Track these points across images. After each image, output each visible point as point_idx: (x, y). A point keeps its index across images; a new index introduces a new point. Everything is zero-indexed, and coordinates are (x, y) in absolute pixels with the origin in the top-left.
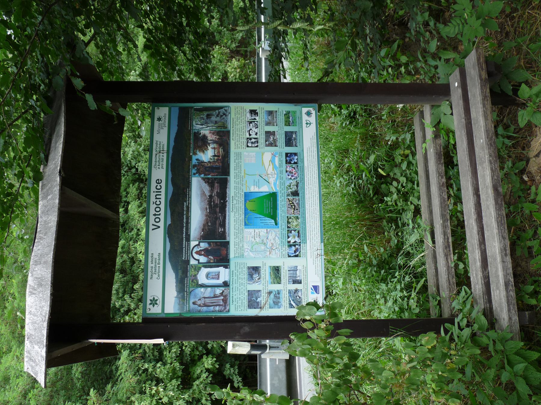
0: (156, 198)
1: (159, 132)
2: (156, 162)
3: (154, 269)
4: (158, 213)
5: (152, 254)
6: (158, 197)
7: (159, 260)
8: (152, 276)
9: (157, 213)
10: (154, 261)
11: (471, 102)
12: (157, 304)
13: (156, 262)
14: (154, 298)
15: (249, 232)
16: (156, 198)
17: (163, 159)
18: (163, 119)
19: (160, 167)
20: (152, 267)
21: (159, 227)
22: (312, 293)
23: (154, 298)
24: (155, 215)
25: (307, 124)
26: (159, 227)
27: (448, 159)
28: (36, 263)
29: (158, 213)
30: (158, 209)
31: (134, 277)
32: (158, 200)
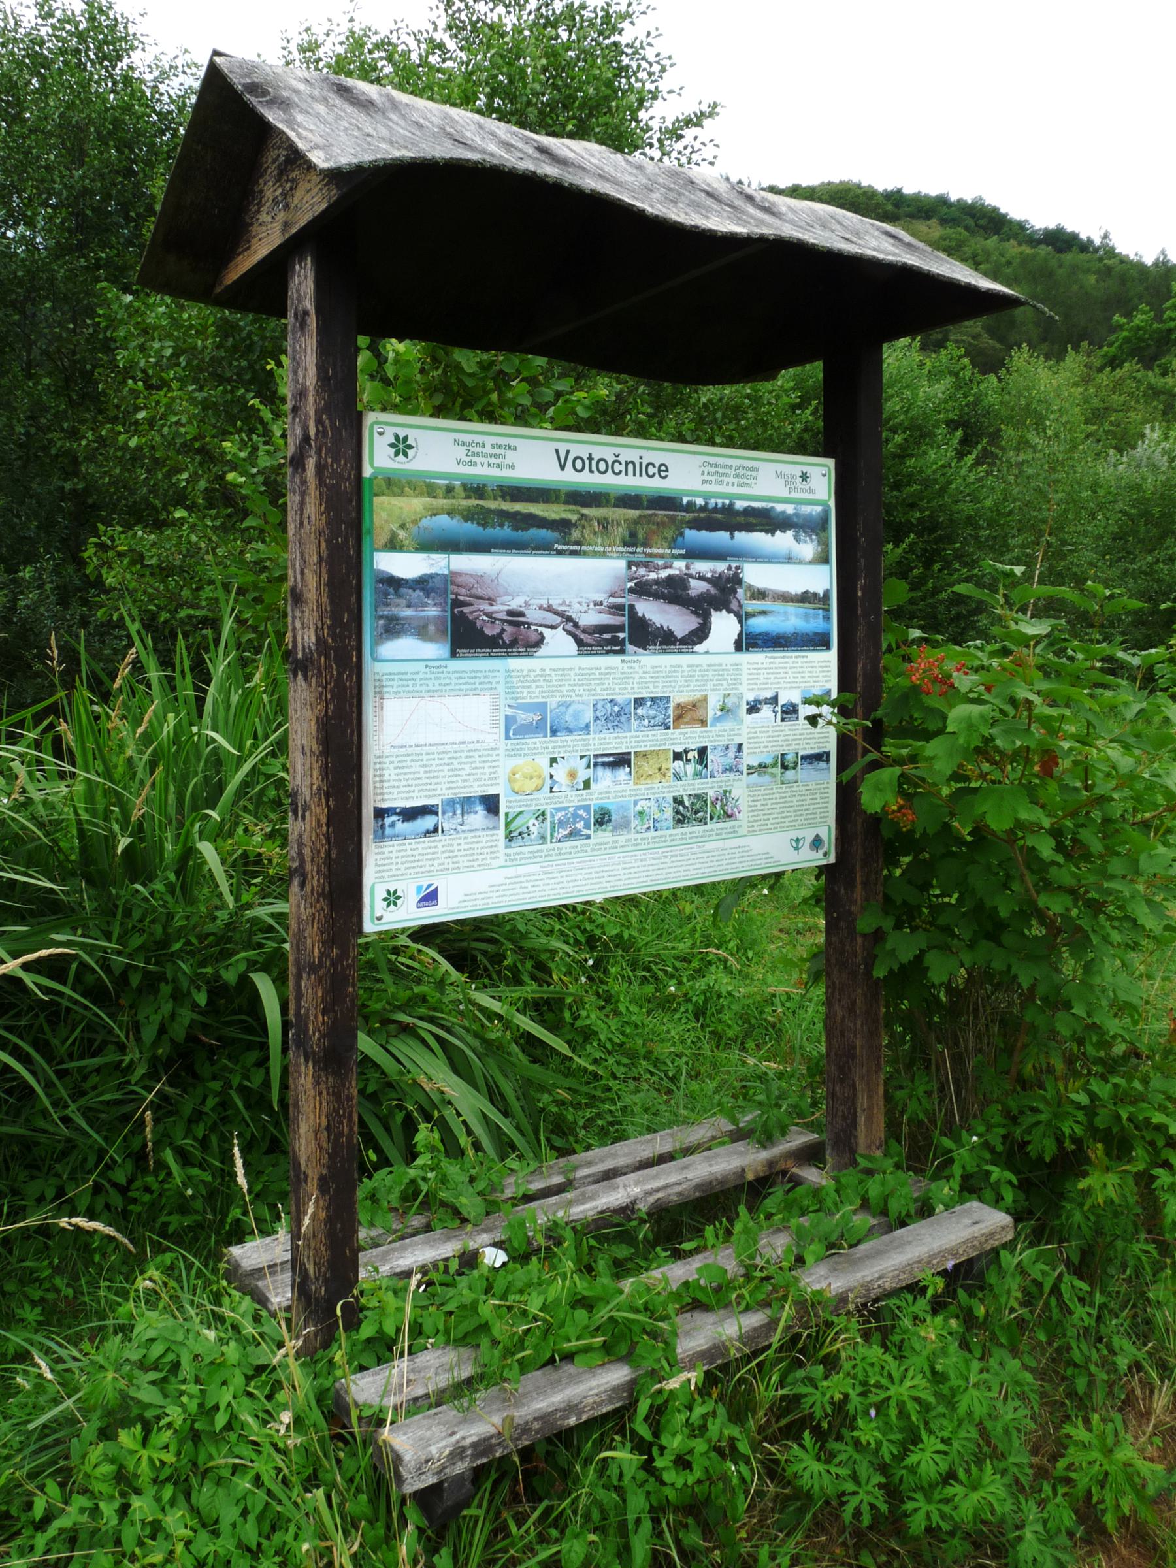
0: (627, 463)
1: (779, 475)
2: (716, 466)
3: (479, 450)
4: (594, 468)
5: (515, 448)
6: (630, 466)
7: (498, 466)
8: (463, 444)
9: (594, 463)
10: (498, 452)
11: (654, 1170)
12: (397, 454)
13: (495, 456)
14: (410, 447)
15: (828, 686)
16: (627, 463)
17: (720, 483)
18: (804, 485)
19: (706, 477)
20: (484, 446)
21: (562, 468)
22: (419, 888)
23: (410, 447)
24: (590, 458)
25: (798, 840)
26: (562, 468)
27: (662, 1159)
28: (226, 329)
29: (594, 468)
30: (602, 466)
31: (454, 401)
32: (622, 468)
